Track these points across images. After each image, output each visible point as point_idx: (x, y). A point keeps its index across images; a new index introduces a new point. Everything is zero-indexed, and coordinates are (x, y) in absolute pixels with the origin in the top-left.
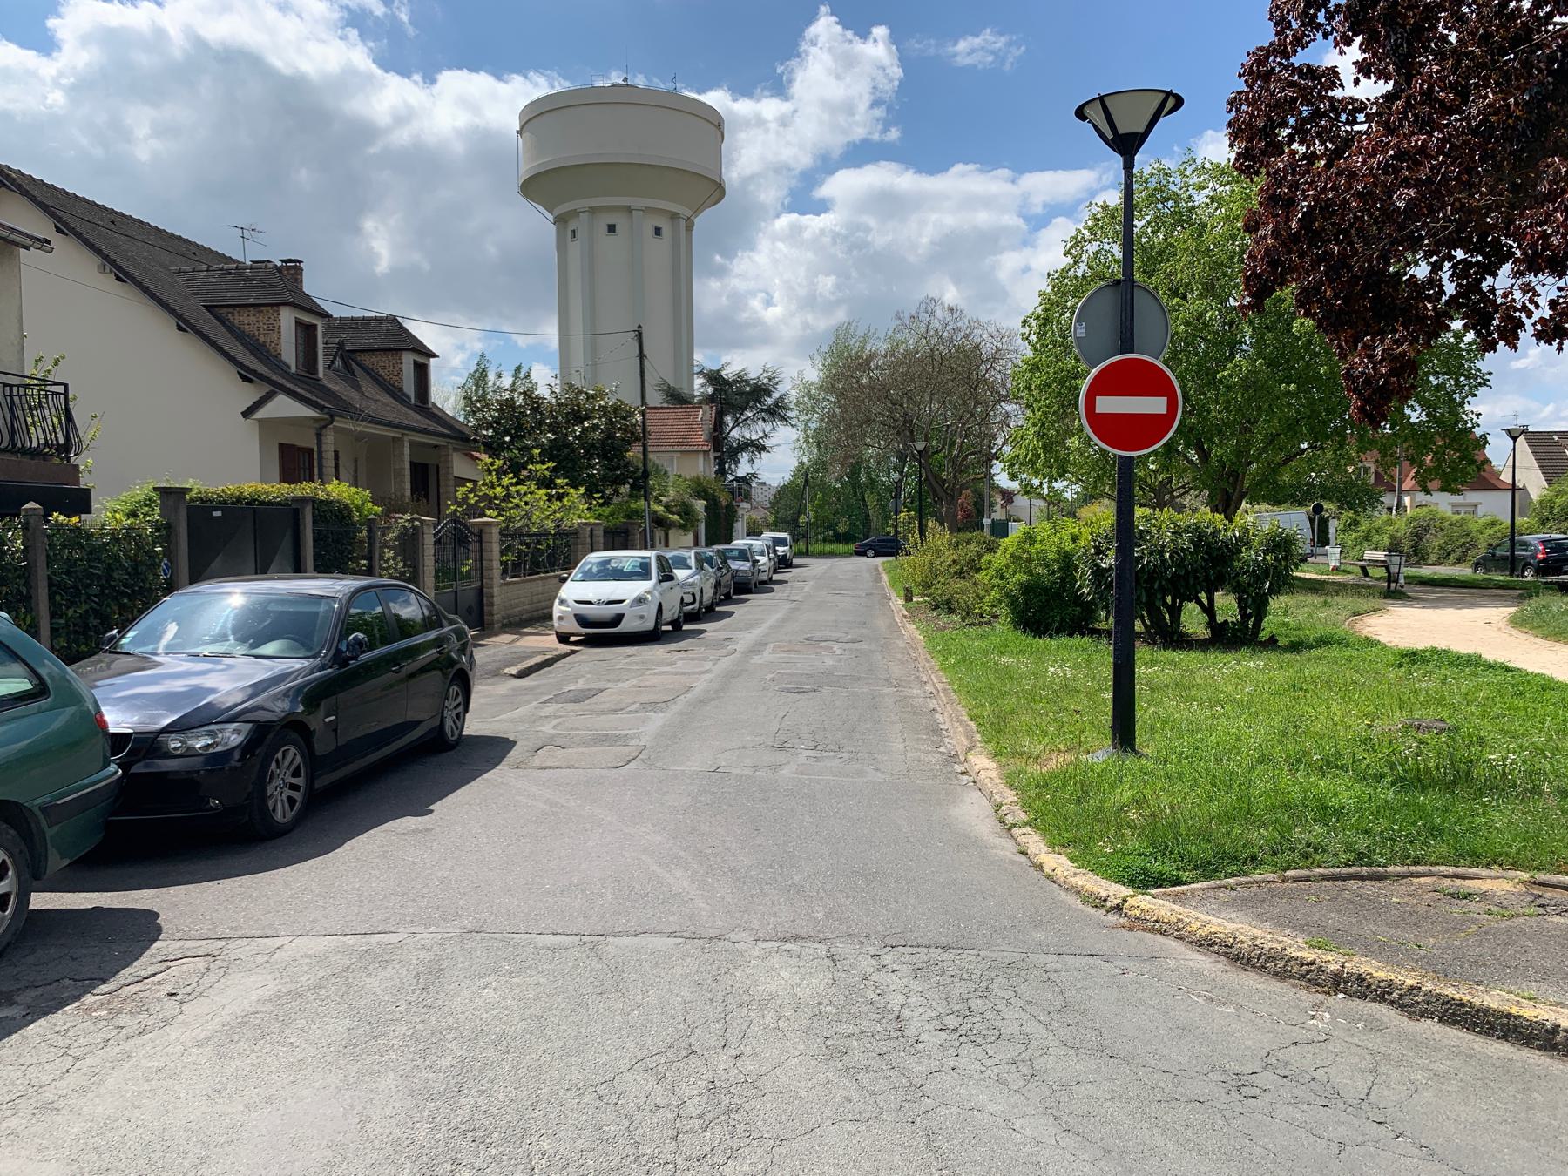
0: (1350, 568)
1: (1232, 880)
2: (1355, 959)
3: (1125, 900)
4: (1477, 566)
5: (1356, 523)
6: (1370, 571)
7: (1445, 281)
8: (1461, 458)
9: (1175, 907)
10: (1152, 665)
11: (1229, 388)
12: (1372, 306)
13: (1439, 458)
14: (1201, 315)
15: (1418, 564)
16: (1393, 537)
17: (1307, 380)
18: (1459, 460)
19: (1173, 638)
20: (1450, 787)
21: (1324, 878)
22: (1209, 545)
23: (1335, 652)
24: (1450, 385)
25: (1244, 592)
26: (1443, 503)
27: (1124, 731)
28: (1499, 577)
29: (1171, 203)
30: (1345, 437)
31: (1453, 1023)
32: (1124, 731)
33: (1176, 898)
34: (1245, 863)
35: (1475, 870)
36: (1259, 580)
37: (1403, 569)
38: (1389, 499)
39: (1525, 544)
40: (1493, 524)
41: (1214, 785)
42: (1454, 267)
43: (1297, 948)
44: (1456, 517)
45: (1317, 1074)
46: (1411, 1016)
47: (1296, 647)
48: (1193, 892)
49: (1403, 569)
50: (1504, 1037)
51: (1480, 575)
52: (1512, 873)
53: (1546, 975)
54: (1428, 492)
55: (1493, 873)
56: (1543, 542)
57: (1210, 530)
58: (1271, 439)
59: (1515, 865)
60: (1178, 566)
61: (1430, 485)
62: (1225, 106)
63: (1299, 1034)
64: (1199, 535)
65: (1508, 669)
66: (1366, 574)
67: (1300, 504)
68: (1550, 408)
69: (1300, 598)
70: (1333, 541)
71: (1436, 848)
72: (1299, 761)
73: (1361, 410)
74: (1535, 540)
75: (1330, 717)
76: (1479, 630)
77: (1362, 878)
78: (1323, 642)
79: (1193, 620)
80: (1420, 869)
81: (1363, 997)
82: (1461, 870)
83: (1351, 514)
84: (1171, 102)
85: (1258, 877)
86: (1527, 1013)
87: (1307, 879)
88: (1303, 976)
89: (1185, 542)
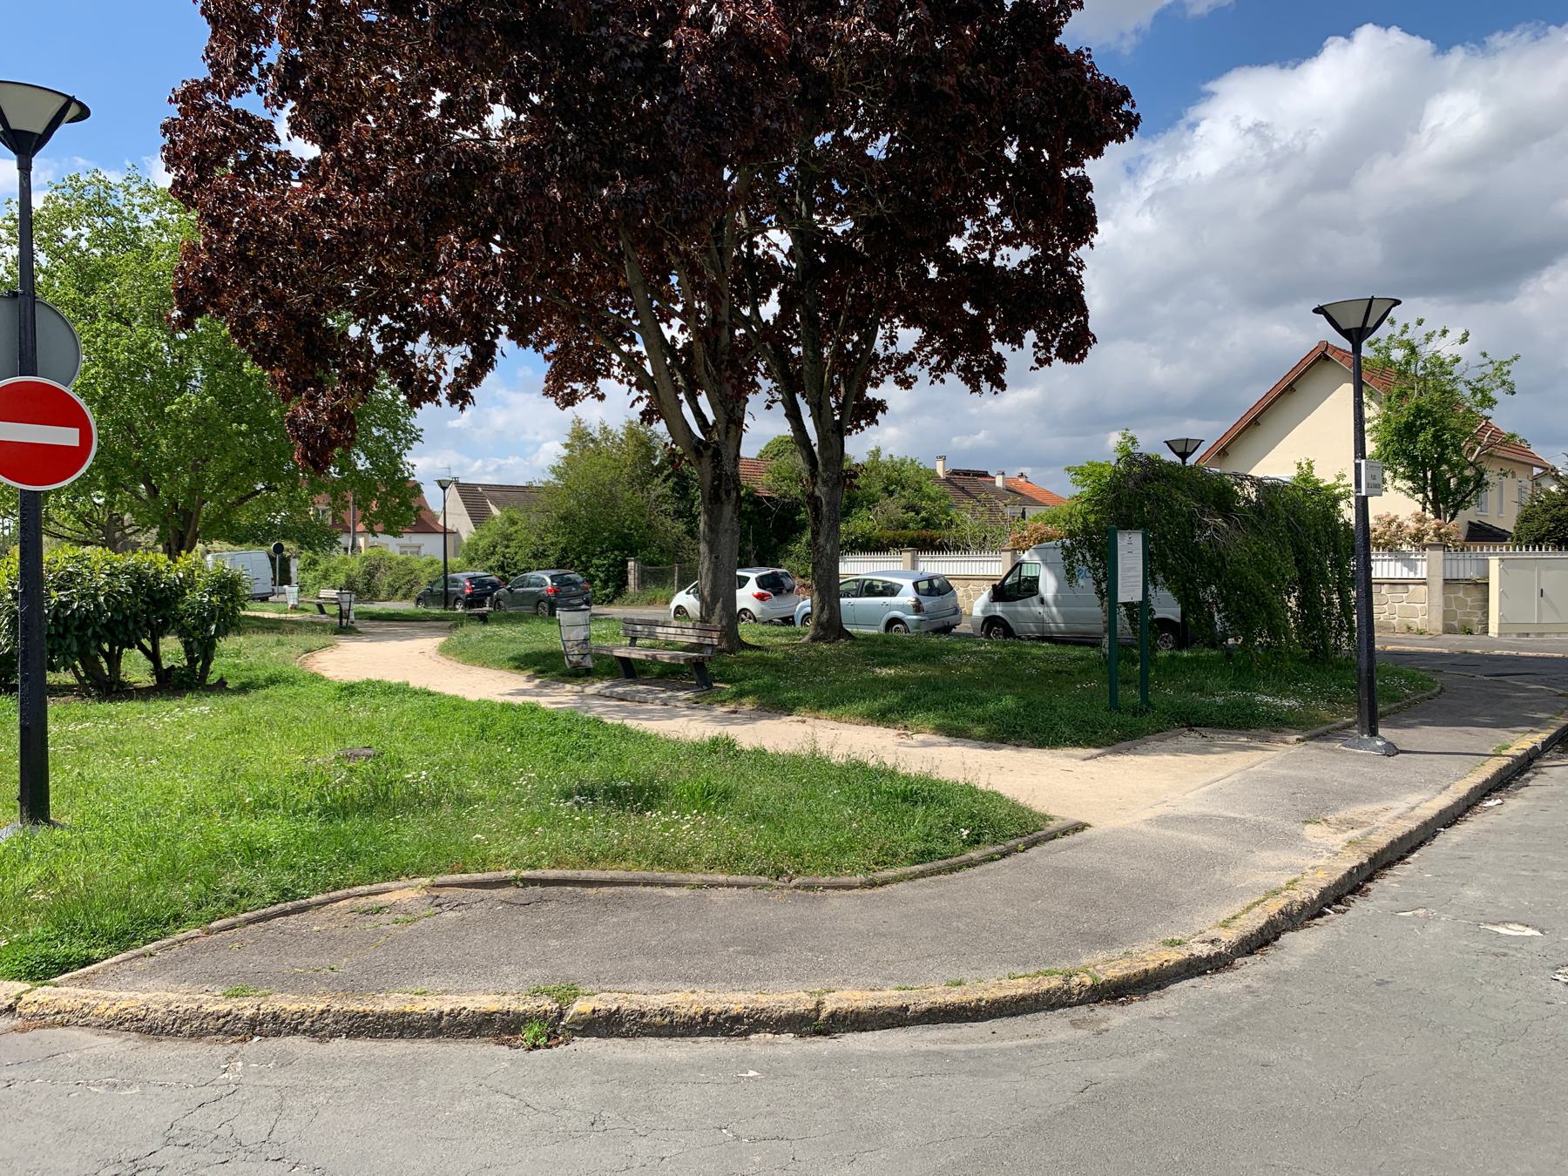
0: (307, 606)
1: (151, 946)
2: (271, 998)
3: (19, 998)
4: (418, 600)
5: (314, 563)
6: (326, 608)
7: (374, 342)
8: (400, 504)
9: (80, 991)
10: (72, 723)
11: (178, 423)
12: (305, 352)
13: (383, 503)
14: (144, 345)
15: (371, 601)
16: (348, 576)
17: (259, 422)
18: (400, 507)
19: (112, 689)
20: (368, 810)
21: (250, 922)
22: (150, 587)
23: (282, 691)
24: (389, 438)
25: (190, 636)
26: (391, 546)
27: (34, 801)
28: (436, 611)
29: (111, 220)
30: (297, 479)
31: (357, 1035)
32: (34, 801)
33: (85, 981)
34: (167, 924)
35: (386, 885)
36: (205, 623)
37: (354, 606)
38: (345, 540)
39: (455, 581)
40: (432, 563)
41: (137, 845)
42: (381, 329)
43: (214, 1002)
44: (403, 557)
45: (219, 1132)
46: (322, 1040)
47: (244, 688)
48: (105, 970)
49: (354, 606)
50: (401, 1036)
51: (421, 609)
52: (415, 881)
53: (436, 968)
54: (374, 534)
55: (401, 884)
56: (470, 579)
57: (152, 571)
58: (225, 480)
59: (420, 873)
60: (114, 610)
61: (376, 528)
62: (159, 131)
63: (208, 1093)
64: (138, 577)
65: (429, 694)
66: (323, 612)
67: (262, 544)
68: (479, 463)
69: (255, 637)
70: (294, 580)
71: (355, 870)
72: (232, 806)
73: (305, 456)
74: (463, 578)
75: (270, 755)
76: (411, 660)
77: (286, 913)
78: (272, 681)
79: (134, 666)
80: (339, 893)
81: (278, 1034)
82: (374, 887)
83: (310, 553)
84: (73, 110)
85: (180, 936)
86: (418, 1008)
87: (233, 927)
88: (219, 1030)
89: (122, 584)
